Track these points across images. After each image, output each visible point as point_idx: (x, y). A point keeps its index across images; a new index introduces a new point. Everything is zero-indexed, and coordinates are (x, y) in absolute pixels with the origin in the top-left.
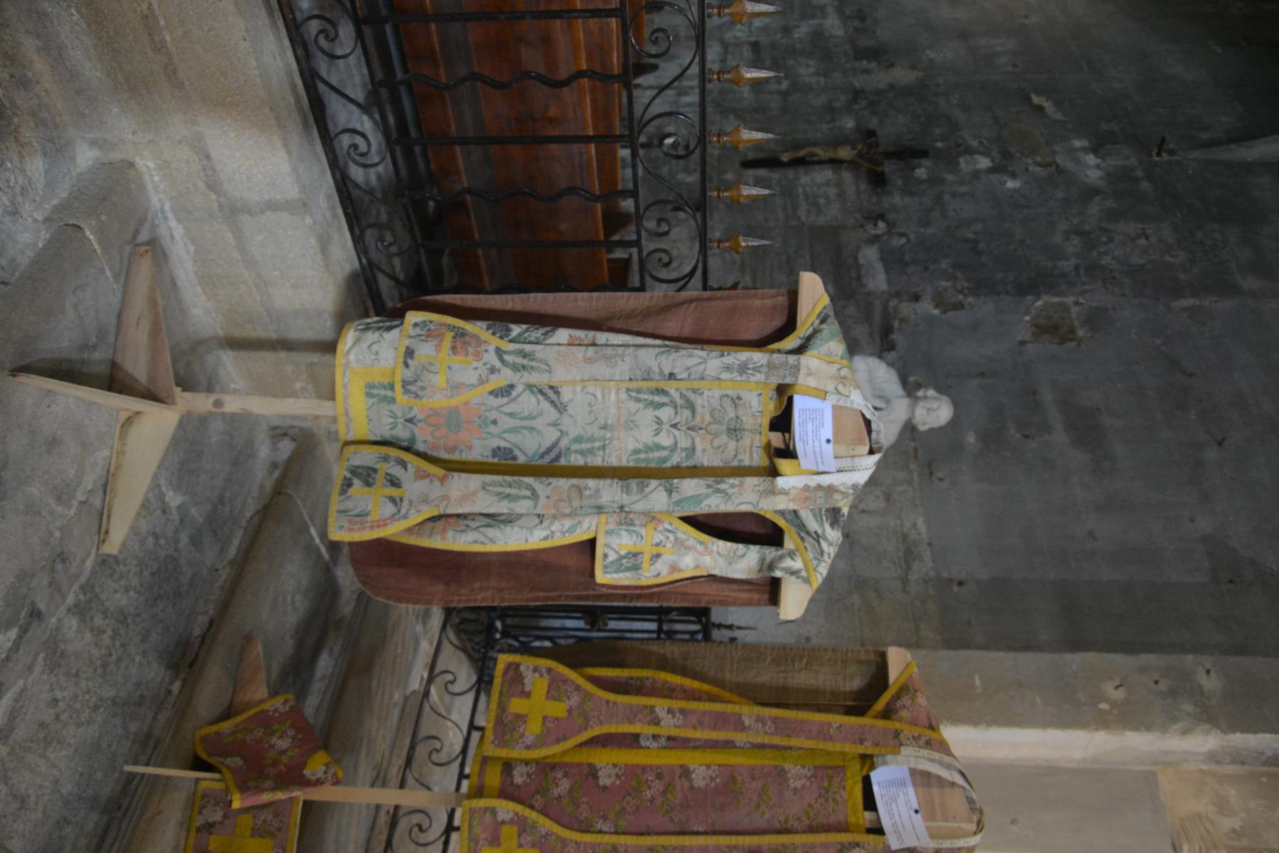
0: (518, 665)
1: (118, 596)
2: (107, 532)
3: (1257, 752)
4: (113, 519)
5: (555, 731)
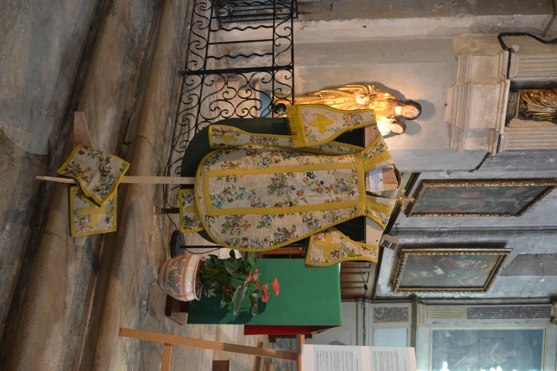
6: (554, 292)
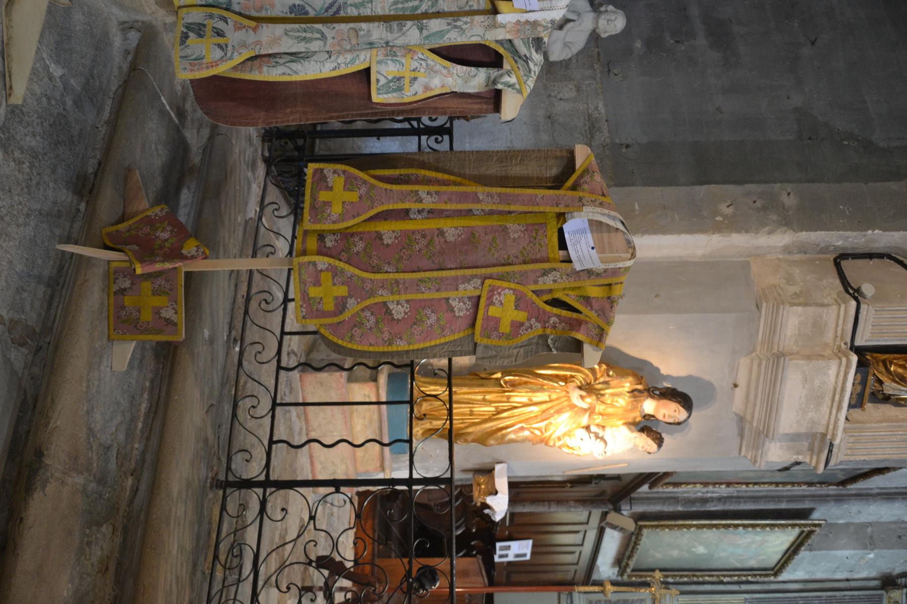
0: (322, 170)
1: (28, 138)
2: (11, 88)
3: (814, 245)
4: (13, 77)
5: (350, 210)
6: (889, 571)
